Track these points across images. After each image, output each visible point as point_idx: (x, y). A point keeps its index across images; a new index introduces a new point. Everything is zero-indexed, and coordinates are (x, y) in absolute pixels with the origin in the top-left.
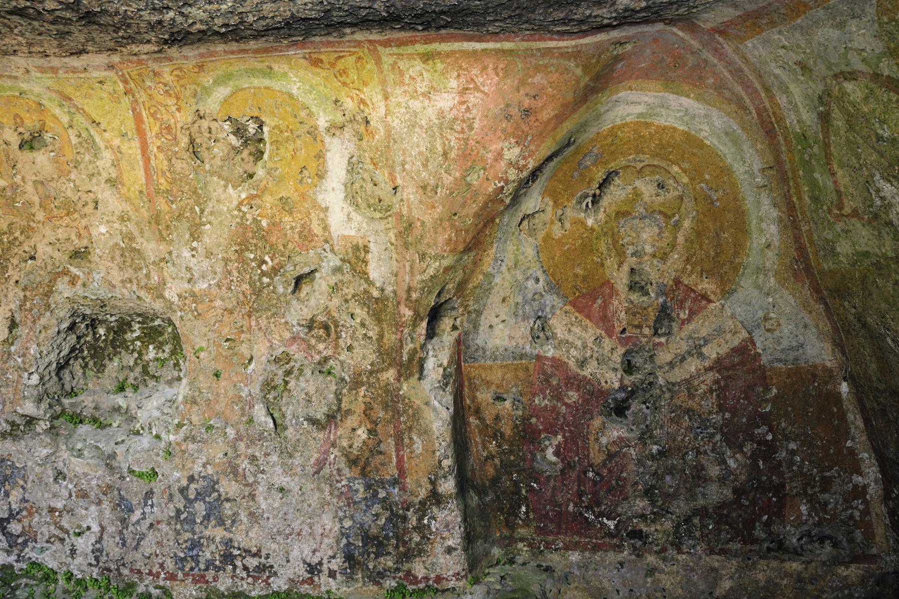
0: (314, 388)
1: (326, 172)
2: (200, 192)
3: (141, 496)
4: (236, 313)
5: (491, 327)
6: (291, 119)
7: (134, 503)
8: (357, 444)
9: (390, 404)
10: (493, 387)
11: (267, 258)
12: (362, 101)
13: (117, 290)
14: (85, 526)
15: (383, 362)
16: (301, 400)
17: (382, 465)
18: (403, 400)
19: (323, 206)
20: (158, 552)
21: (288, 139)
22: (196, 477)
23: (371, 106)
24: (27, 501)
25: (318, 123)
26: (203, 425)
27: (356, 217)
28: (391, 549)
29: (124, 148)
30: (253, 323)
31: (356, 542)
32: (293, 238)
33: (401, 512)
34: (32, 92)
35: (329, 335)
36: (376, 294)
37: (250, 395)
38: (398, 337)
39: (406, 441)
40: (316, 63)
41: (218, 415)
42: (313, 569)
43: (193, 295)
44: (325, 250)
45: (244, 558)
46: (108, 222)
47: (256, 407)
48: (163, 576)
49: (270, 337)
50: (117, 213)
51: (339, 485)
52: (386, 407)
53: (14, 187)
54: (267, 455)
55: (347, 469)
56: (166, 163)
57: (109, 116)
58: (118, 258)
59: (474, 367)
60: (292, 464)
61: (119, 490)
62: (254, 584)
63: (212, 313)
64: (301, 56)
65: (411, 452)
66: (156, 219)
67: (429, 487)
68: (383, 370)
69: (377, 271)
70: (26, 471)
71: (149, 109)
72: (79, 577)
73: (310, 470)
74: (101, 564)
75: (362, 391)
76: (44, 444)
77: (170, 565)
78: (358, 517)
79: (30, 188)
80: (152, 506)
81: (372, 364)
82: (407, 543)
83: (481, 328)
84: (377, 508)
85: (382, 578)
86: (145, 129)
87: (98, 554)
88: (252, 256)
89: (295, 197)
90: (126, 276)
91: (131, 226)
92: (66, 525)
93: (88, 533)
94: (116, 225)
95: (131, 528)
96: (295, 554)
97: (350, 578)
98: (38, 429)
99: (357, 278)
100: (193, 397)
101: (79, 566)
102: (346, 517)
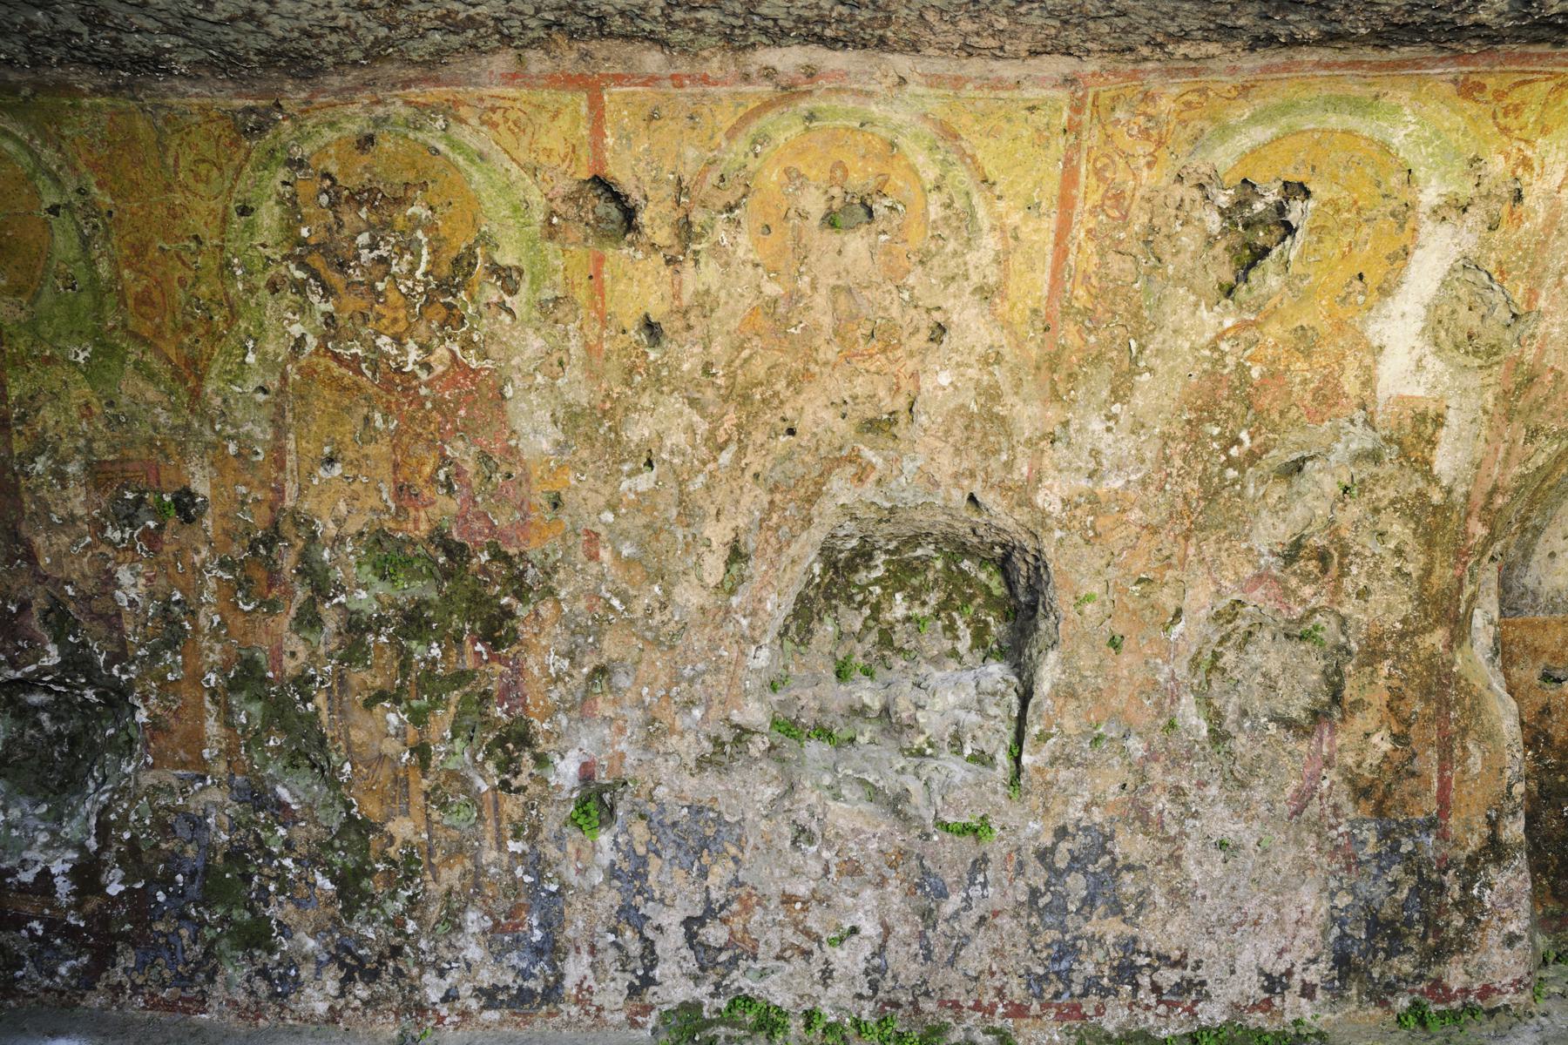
0: (1278, 664)
1: (1399, 284)
2: (1146, 314)
3: (963, 869)
4: (1164, 532)
5: (1552, 555)
6: (1366, 190)
7: (948, 880)
8: (1373, 759)
9: (1434, 689)
10: (1545, 659)
11: (1244, 435)
12: (1526, 163)
13: (941, 492)
14: (847, 926)
15: (1426, 616)
16: (1255, 686)
17: (1413, 795)
18: (1458, 682)
19: (1376, 344)
20: (994, 968)
21: (1345, 224)
22: (1071, 829)
23: (1537, 170)
24: (742, 885)
25: (1421, 197)
26: (1084, 734)
27: (1434, 364)
28: (1412, 942)
29: (1025, 232)
30: (1192, 551)
31: (1356, 933)
32: (1302, 399)
33: (1435, 876)
34: (886, 120)
35: (1324, 571)
36: (1437, 497)
37: (1173, 679)
38: (1458, 572)
39: (1458, 752)
40: (1469, 89)
41: (1114, 716)
42: (1274, 984)
43: (1094, 500)
44: (1352, 422)
45: (1156, 969)
46: (958, 365)
47: (1183, 701)
48: (1001, 1010)
49: (1217, 576)
50: (979, 349)
51: (1334, 833)
52: (1426, 693)
53: (794, 297)
54: (1202, 784)
55: (1351, 805)
56: (1095, 259)
57: (1018, 170)
58: (956, 432)
59: (1513, 624)
60: (1248, 799)
61: (920, 858)
62: (1167, 1017)
63: (1121, 532)
64: (1451, 77)
65: (1464, 772)
66: (1053, 361)
67: (1486, 831)
68: (1424, 630)
69: (1446, 460)
70: (743, 828)
71: (1095, 160)
72: (833, 1019)
73: (1283, 808)
74: (881, 994)
75: (1385, 668)
76: (768, 778)
77: (1016, 990)
78: (1364, 887)
79: (821, 300)
80: (984, 885)
81: (1404, 621)
82: (1441, 930)
83: (1535, 558)
84: (1396, 871)
85: (1392, 994)
86: (1075, 197)
87: (877, 976)
88: (1216, 431)
89: (1325, 327)
90: (965, 464)
91: (1001, 374)
92: (816, 927)
93: (855, 939)
94: (972, 372)
95: (942, 927)
96: (1246, 957)
97: (1338, 995)
98: (754, 751)
99: (1408, 471)
100: (1069, 685)
101: (834, 1002)
102: (1341, 889)
